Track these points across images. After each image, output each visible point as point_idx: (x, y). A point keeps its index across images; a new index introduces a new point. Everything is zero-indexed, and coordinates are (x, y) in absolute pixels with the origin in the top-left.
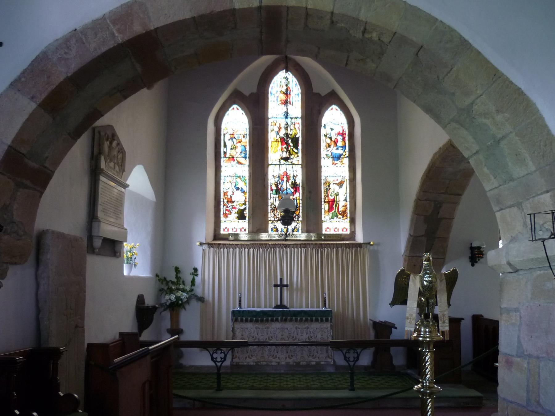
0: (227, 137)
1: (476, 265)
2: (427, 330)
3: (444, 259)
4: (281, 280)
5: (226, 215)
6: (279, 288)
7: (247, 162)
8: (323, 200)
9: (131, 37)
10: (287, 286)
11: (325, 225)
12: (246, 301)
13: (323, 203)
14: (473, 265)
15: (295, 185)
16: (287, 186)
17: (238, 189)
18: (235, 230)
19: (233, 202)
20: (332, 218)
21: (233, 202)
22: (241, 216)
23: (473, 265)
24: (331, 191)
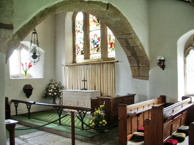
0: (78, 23)
1: (165, 69)
2: (104, 121)
3: (149, 66)
4: (84, 78)
5: (77, 53)
6: (83, 82)
7: (83, 32)
8: (108, 43)
9: (184, 44)
10: (82, 81)
11: (109, 54)
12: (108, 79)
13: (108, 44)
14: (163, 69)
15: (99, 39)
16: (96, 40)
17: (81, 43)
18: (96, 57)
19: (79, 48)
20: (112, 50)
21: (79, 48)
22: (82, 54)
23: (163, 69)
24: (111, 38)
